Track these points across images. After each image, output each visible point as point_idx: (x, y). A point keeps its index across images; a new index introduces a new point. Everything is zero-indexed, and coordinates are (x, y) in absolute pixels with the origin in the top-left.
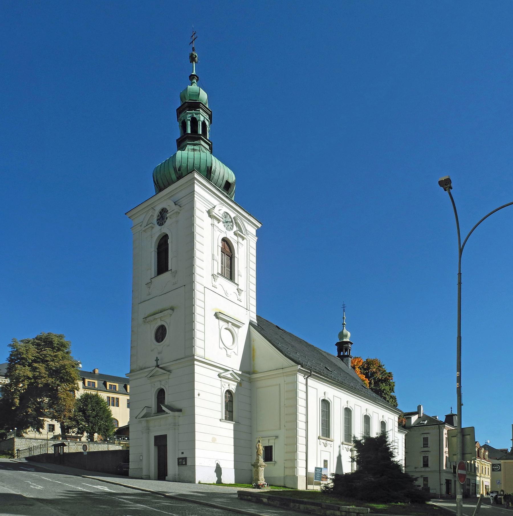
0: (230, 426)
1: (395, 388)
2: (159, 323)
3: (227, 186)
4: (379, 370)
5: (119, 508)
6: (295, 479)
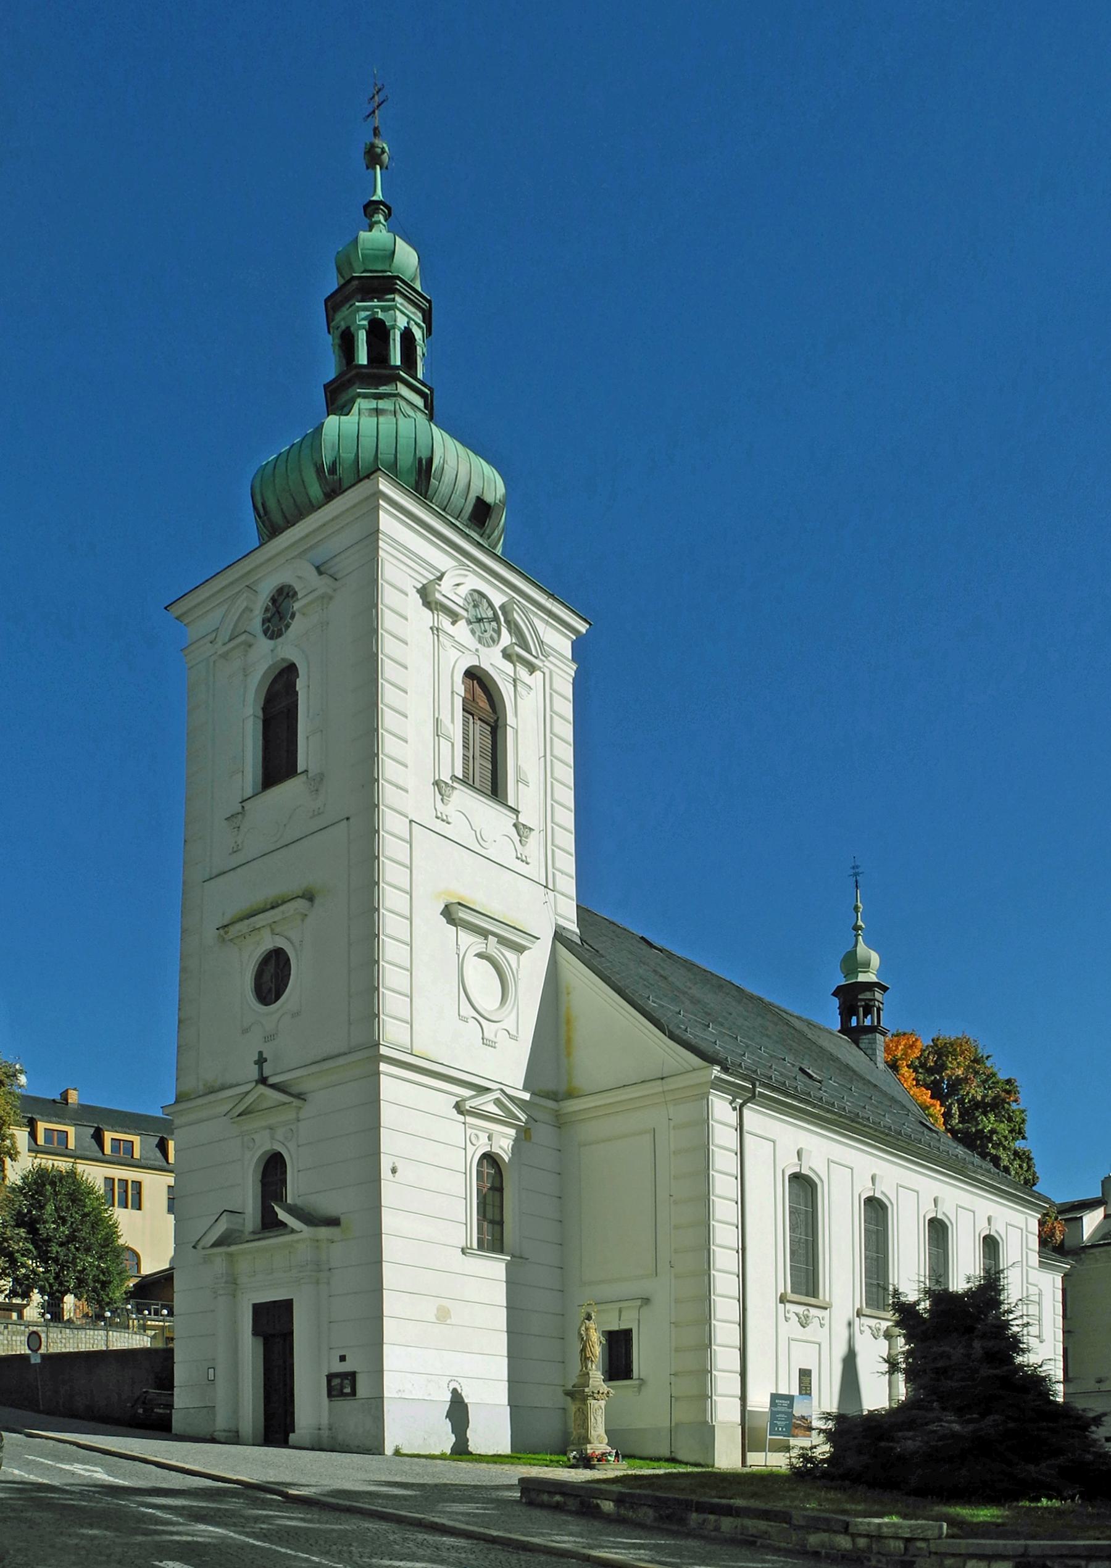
0: (494, 1270)
1: (1028, 1128)
2: (268, 943)
3: (482, 513)
4: (976, 1073)
5: (140, 1538)
6: (706, 1433)
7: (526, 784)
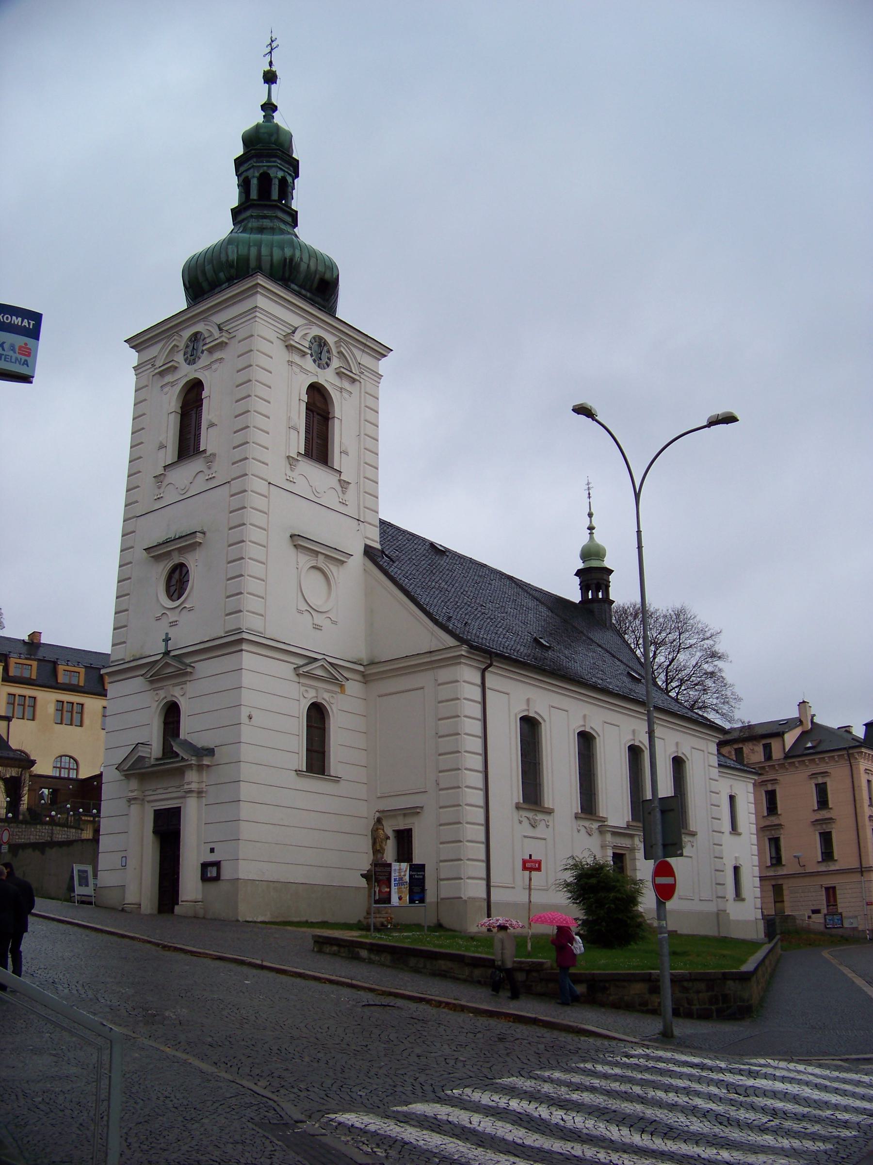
7: (347, 453)
